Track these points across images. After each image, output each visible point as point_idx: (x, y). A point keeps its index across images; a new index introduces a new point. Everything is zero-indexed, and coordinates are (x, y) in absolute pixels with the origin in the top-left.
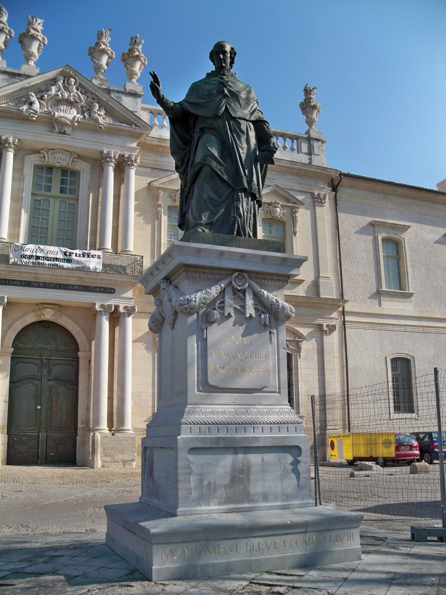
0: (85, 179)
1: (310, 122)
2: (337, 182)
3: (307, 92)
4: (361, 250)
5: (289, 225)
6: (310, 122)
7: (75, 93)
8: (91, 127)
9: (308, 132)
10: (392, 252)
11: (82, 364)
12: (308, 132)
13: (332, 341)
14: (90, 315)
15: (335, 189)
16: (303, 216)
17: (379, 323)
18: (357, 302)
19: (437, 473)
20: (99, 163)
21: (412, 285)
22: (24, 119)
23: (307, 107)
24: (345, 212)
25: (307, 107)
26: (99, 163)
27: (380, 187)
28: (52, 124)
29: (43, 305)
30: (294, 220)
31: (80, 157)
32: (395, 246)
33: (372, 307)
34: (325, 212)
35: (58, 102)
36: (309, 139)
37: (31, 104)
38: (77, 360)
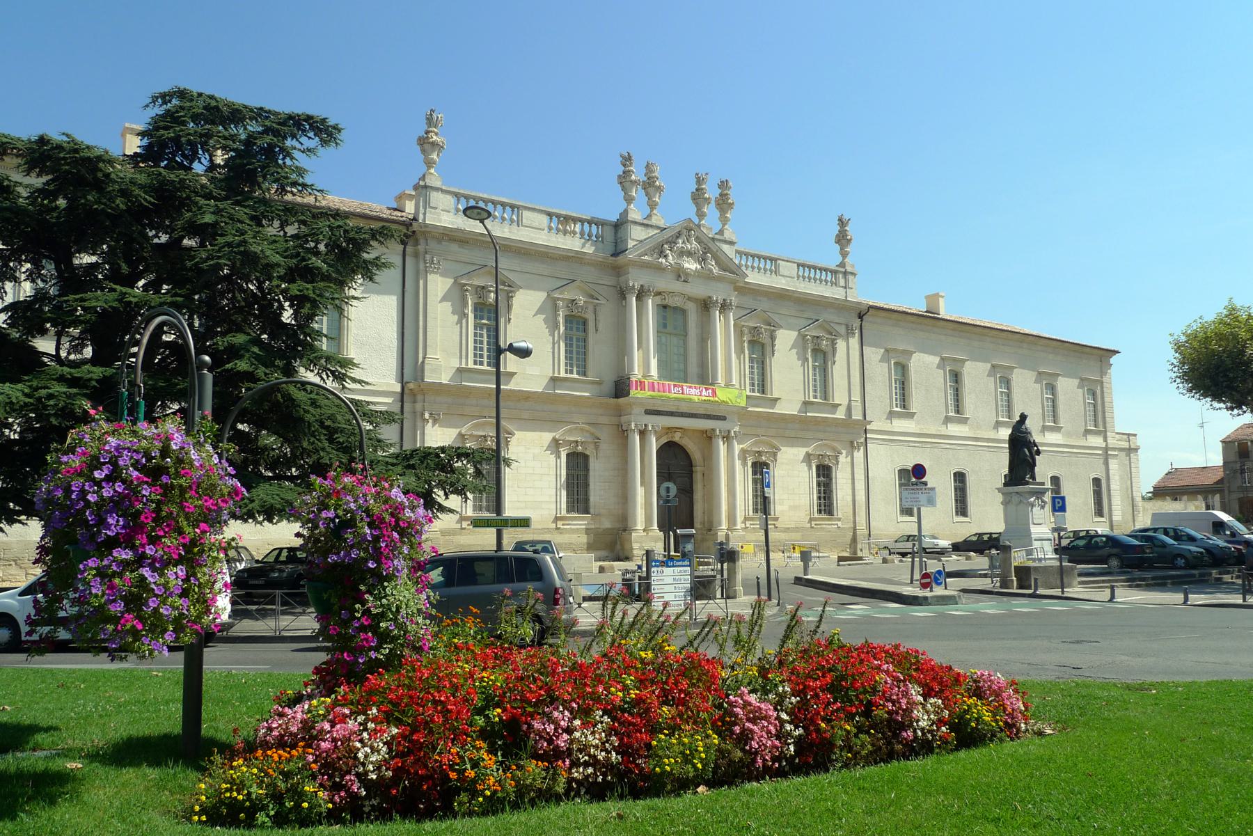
0: (693, 318)
1: (844, 254)
2: (863, 313)
3: (842, 223)
4: (880, 373)
5: (830, 355)
6: (844, 254)
7: (693, 245)
8: (706, 276)
9: (842, 265)
10: (900, 373)
11: (698, 477)
12: (842, 265)
13: (859, 455)
14: (708, 437)
15: (861, 317)
16: (841, 345)
17: (892, 439)
18: (878, 423)
19: (173, 707)
20: (705, 305)
21: (915, 405)
22: (660, 269)
23: (843, 239)
24: (870, 346)
25: (843, 239)
26: (705, 305)
27: (895, 316)
28: (680, 275)
29: (670, 430)
30: (834, 350)
31: (689, 299)
32: (903, 369)
33: (886, 426)
34: (854, 342)
35: (683, 253)
36: (845, 273)
37: (666, 256)
38: (692, 472)
